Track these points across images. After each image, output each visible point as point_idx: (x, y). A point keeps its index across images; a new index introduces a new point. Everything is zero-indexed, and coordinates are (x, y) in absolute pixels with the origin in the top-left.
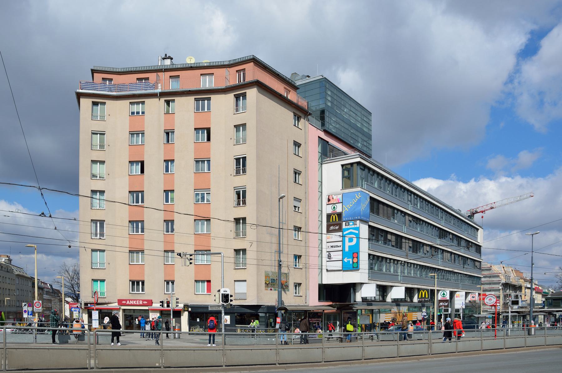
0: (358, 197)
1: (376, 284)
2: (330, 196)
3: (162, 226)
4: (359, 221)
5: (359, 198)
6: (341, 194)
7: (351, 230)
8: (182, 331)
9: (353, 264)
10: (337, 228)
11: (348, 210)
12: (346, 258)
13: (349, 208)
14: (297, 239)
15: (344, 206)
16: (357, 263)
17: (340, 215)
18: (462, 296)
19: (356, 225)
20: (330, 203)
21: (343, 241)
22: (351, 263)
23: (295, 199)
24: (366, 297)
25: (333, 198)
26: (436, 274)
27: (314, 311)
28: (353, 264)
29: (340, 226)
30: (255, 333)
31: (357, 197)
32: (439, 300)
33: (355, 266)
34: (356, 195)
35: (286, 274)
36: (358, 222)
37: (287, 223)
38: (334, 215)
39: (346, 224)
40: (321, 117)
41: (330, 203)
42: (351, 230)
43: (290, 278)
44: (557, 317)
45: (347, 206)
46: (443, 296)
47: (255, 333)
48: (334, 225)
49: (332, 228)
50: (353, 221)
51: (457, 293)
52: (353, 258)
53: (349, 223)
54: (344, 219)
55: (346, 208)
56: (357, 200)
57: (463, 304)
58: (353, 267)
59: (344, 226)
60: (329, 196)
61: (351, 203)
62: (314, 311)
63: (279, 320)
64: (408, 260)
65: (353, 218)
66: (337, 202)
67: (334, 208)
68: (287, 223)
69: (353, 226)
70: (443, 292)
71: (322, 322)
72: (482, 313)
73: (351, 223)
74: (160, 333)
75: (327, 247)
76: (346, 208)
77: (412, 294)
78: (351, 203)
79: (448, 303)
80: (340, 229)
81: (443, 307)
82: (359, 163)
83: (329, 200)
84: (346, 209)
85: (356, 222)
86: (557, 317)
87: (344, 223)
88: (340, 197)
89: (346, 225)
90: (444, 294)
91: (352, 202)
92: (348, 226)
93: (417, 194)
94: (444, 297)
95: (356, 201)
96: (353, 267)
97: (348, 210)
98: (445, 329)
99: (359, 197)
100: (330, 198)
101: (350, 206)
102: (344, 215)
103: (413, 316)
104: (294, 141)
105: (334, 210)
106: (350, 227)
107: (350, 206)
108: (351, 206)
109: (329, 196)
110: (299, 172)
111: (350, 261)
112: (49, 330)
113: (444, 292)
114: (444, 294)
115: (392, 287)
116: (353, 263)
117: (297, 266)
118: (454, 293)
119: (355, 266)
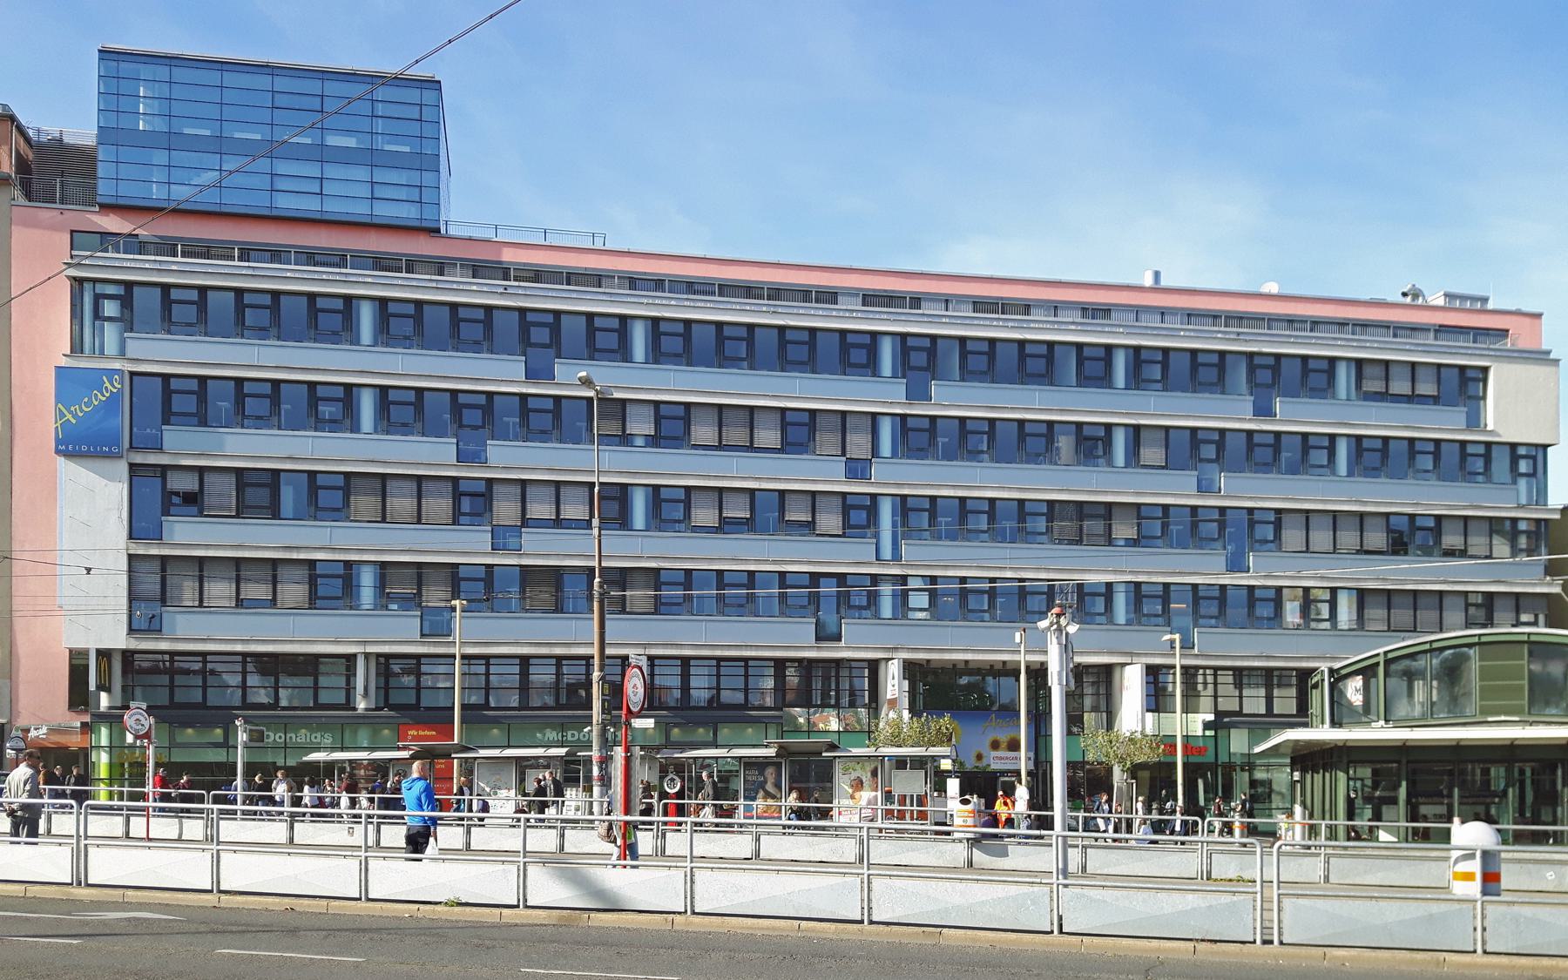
0: (110, 387)
5: (115, 391)
11: (74, 421)
13: (81, 415)
27: (1516, 719)
30: (884, 834)
31: (107, 384)
34: (104, 378)
44: (761, 794)
47: (884, 834)
55: (66, 412)
56: (108, 395)
61: (86, 400)
62: (1516, 719)
63: (439, 764)
71: (877, 776)
74: (101, 245)
76: (66, 412)
78: (86, 400)
84: (69, 416)
86: (761, 794)
91: (90, 399)
93: (1169, 363)
97: (74, 421)
98: (1145, 814)
99: (104, 396)
101: (82, 411)
103: (1327, 775)
107: (82, 411)
112: (306, 806)
117: (1278, 416)
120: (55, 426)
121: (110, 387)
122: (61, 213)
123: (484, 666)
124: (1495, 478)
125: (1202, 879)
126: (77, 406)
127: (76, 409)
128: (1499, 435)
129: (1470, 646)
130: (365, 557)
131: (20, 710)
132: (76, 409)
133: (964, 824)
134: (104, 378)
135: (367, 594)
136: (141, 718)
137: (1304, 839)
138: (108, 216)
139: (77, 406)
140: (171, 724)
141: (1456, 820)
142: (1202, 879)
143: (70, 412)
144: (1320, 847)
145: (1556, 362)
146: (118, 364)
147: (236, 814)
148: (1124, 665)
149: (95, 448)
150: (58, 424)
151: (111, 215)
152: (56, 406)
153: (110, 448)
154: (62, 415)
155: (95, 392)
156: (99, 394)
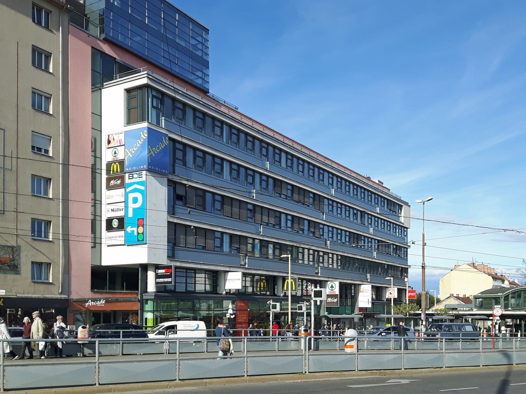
0: (143, 137)
1: (242, 272)
2: (110, 136)
3: (148, 221)
4: (145, 171)
6: (124, 133)
7: (136, 186)
8: (177, 329)
9: (138, 236)
10: (119, 182)
11: (154, 155)
12: (130, 227)
14: (42, 195)
15: (126, 150)
16: (143, 233)
17: (121, 163)
18: (367, 291)
19: (142, 177)
20: (110, 146)
21: (126, 202)
22: (136, 234)
23: (34, 133)
24: (230, 290)
25: (114, 140)
26: (290, 256)
28: (138, 236)
29: (122, 178)
31: (142, 136)
32: (328, 295)
33: (140, 239)
34: (141, 133)
35: (12, 247)
36: (144, 172)
37: (14, 169)
38: (115, 163)
39: (129, 177)
40: (100, 19)
41: (110, 146)
42: (136, 186)
43: (22, 254)
45: (131, 150)
46: (331, 289)
48: (115, 178)
49: (112, 182)
50: (138, 172)
51: (362, 286)
52: (138, 227)
53: (133, 174)
54: (127, 169)
56: (142, 141)
57: (369, 302)
58: (138, 240)
59: (127, 181)
60: (109, 136)
61: (135, 145)
64: (478, 271)
65: (138, 168)
66: (119, 145)
67: (115, 153)
68: (14, 169)
69: (138, 180)
70: (331, 284)
72: (303, 311)
73: (135, 176)
75: (107, 211)
76: (152, 151)
77: (380, 292)
78: (135, 145)
79: (338, 299)
80: (123, 185)
81: (271, 302)
82: (146, 86)
83: (109, 142)
84: (130, 154)
85: (142, 173)
87: (127, 175)
88: (122, 137)
89: (129, 179)
90: (332, 287)
92: (132, 180)
94: (332, 290)
95: (163, 147)
96: (138, 240)
97: (131, 156)
99: (145, 136)
100: (110, 139)
101: (134, 150)
102: (126, 163)
104: (32, 45)
105: (115, 156)
106: (134, 181)
108: (135, 149)
109: (109, 136)
110: (47, 95)
111: (134, 231)
113: (333, 284)
114: (332, 287)
115: (226, 273)
116: (138, 233)
118: (324, 282)
119: (140, 239)
120: (147, 156)
121: (143, 137)
122: (89, 36)
123: (196, 277)
124: (207, 210)
125: (166, 353)
126: (155, 148)
127: (154, 149)
128: (404, 225)
129: (522, 291)
130: (227, 231)
131: (72, 291)
132: (154, 149)
133: (84, 337)
134: (141, 133)
135: (226, 248)
136: (498, 310)
137: (509, 336)
138: (105, 44)
139: (155, 148)
140: (178, 300)
141: (347, 329)
142: (166, 353)
143: (153, 151)
144: (420, 339)
145: (409, 206)
146: (164, 131)
147: (460, 340)
148: (361, 284)
149: (160, 170)
150: (149, 155)
151: (106, 44)
152: (148, 146)
153: (165, 171)
154: (150, 152)
155: (138, 140)
156: (161, 144)
